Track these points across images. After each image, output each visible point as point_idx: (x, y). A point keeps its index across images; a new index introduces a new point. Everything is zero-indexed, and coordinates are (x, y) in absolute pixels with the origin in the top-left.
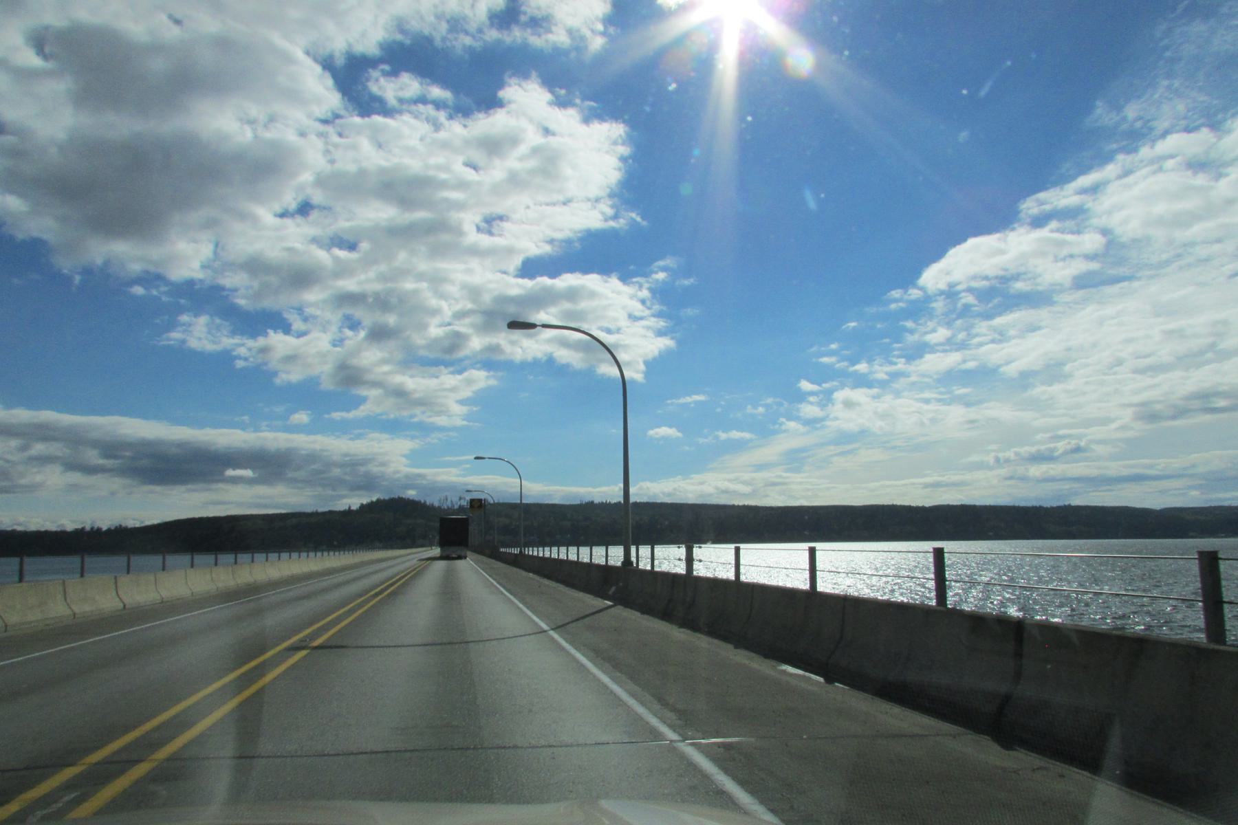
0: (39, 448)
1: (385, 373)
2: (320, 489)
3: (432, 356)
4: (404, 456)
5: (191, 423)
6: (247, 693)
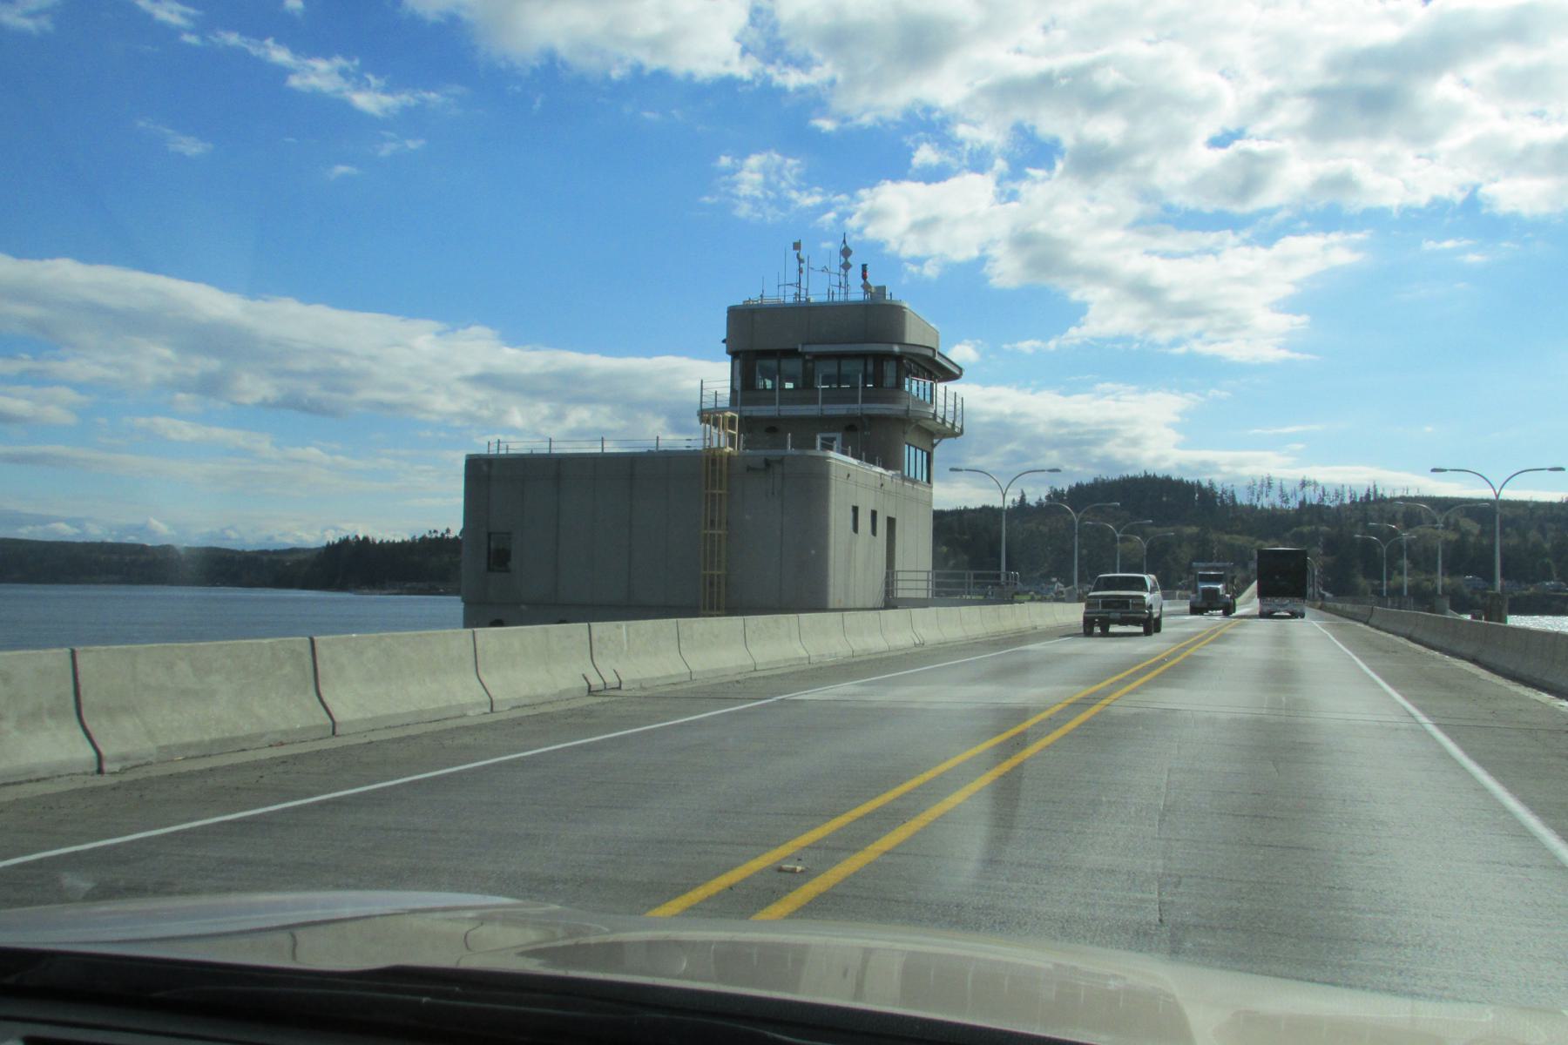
1: (191, 32)
4: (1170, 425)
6: (1006, 766)
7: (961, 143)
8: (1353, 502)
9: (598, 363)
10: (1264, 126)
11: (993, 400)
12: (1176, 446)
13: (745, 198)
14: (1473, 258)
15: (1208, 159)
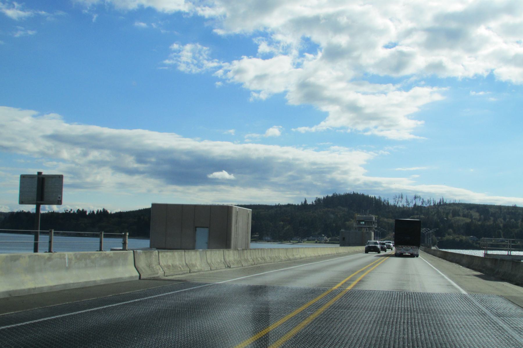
0: (95, 154)
2: (298, 192)
3: (382, 74)
4: (361, 166)
5: (186, 135)
7: (279, 42)
8: (434, 205)
9: (107, 131)
10: (408, 41)
11: (286, 152)
12: (364, 175)
13: (184, 63)
14: (492, 99)
15: (382, 53)
